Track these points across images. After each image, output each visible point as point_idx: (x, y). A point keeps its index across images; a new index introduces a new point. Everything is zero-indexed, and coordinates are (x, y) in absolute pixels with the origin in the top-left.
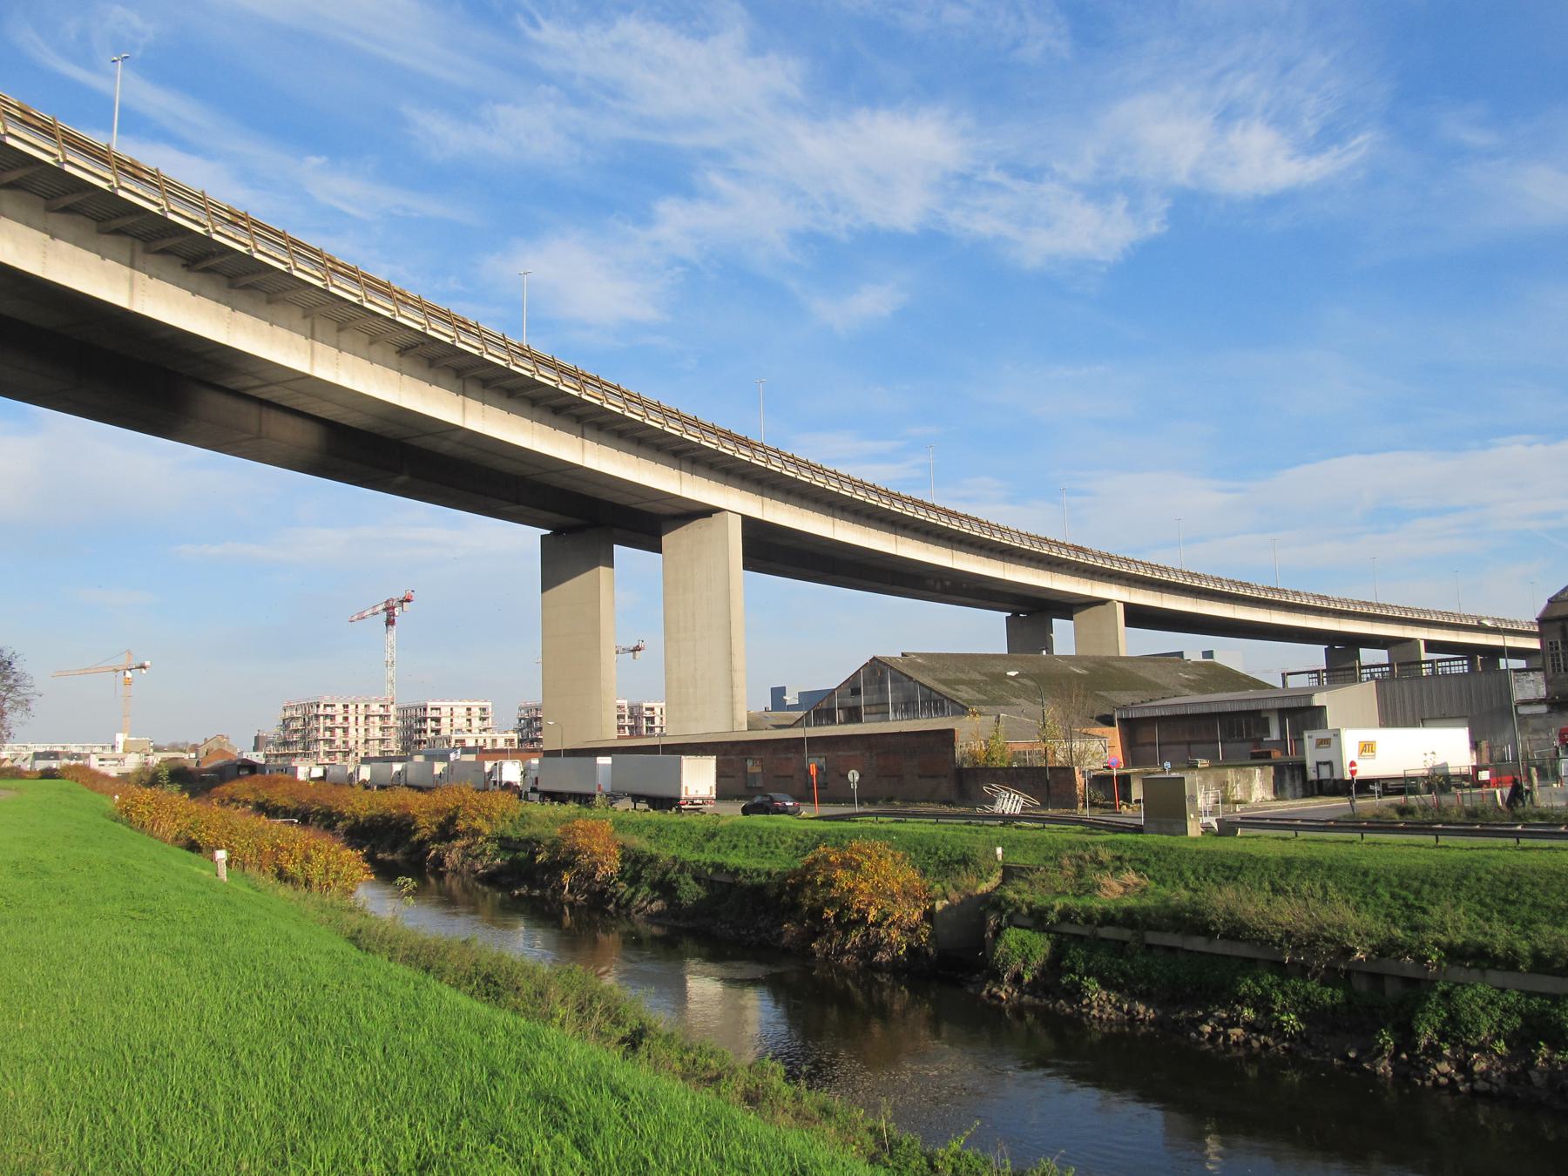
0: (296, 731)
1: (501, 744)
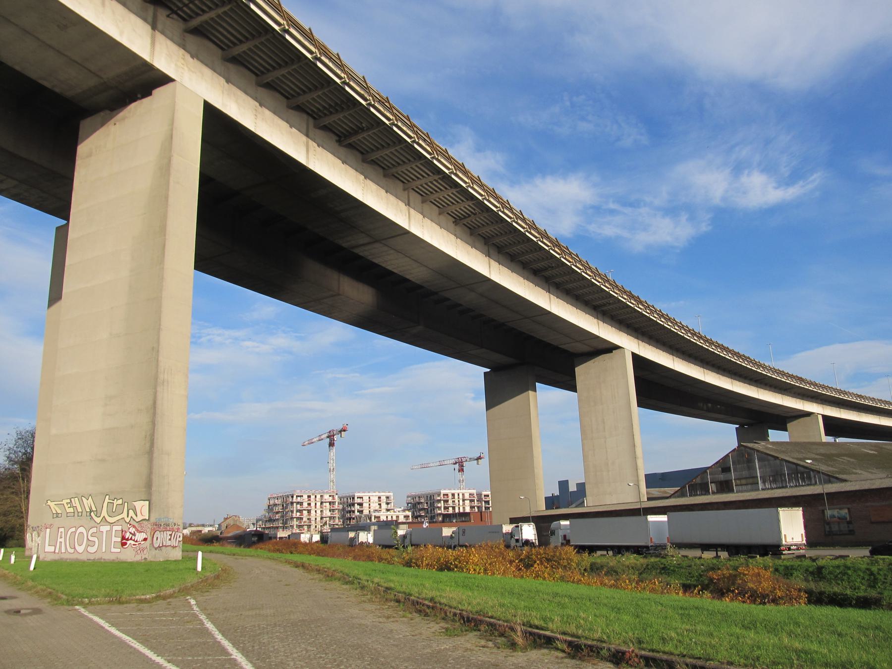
0: (277, 513)
1: (402, 519)
